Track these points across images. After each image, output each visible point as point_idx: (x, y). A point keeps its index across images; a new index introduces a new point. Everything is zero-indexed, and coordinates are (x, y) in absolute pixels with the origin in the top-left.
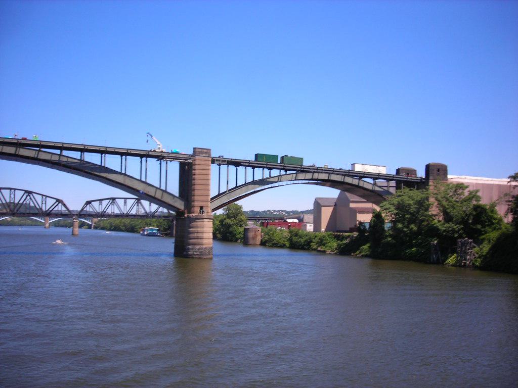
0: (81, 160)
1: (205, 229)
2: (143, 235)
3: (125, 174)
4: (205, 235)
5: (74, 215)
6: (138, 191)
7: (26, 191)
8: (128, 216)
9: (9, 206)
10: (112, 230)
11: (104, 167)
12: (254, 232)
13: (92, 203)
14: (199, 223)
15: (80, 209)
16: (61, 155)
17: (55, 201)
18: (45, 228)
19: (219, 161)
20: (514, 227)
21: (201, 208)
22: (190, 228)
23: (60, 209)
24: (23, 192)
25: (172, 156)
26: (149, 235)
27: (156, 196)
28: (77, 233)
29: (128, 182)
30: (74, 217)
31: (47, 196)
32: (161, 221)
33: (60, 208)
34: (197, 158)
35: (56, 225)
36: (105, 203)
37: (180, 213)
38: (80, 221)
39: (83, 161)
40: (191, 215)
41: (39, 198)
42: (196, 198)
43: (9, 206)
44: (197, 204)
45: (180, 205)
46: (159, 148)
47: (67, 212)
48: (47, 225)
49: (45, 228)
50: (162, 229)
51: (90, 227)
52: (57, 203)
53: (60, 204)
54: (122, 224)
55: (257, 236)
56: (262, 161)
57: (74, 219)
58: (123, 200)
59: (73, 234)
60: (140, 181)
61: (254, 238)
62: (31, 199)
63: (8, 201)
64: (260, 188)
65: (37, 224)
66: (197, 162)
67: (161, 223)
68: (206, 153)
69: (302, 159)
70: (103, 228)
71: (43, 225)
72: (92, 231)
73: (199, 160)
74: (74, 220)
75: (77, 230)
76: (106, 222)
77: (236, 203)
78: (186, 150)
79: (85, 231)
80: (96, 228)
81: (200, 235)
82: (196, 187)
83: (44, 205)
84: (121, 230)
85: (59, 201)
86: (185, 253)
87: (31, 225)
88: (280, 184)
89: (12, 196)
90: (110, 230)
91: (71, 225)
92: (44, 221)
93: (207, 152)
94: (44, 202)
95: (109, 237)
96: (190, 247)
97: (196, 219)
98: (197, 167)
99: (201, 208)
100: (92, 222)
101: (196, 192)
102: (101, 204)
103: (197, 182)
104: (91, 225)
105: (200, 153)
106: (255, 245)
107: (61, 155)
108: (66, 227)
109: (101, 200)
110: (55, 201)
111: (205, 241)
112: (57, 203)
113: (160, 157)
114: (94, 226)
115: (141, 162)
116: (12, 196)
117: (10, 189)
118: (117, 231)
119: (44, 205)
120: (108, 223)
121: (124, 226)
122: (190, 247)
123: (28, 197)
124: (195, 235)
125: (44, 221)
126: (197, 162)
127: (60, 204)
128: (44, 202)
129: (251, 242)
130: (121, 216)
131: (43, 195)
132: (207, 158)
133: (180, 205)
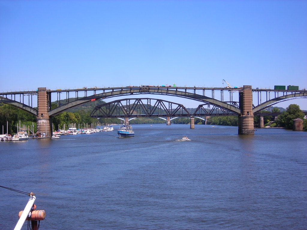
0: (194, 94)
1: (249, 122)
3: (214, 99)
4: (250, 124)
5: (191, 115)
6: (220, 106)
10: (222, 125)
11: (205, 96)
12: (298, 123)
14: (247, 119)
16: (185, 92)
17: (178, 105)
18: (167, 125)
19: (258, 90)
20: (50, 129)
21: (248, 112)
22: (243, 121)
25: (236, 89)
27: (228, 108)
28: (193, 127)
29: (215, 102)
30: (191, 116)
31: (172, 103)
34: (245, 90)
35: (174, 122)
37: (240, 115)
38: (196, 119)
39: (195, 94)
40: (243, 116)
42: (245, 108)
44: (246, 111)
45: (239, 111)
46: (228, 86)
47: (187, 113)
48: (169, 122)
49: (167, 125)
51: (203, 123)
52: (179, 107)
54: (229, 120)
55: (300, 125)
56: (278, 88)
57: (191, 117)
59: (191, 128)
60: (221, 102)
61: (299, 126)
62: (161, 104)
64: (275, 103)
66: (245, 92)
68: (249, 88)
69: (298, 87)
70: (214, 124)
71: (166, 122)
72: (206, 126)
73: (246, 91)
74: (192, 118)
75: (193, 125)
78: (240, 85)
79: (199, 126)
80: (209, 123)
81: (247, 124)
82: (245, 103)
84: (228, 125)
86: (241, 133)
87: (154, 123)
88: (286, 99)
90: (220, 124)
91: (189, 122)
92: (166, 120)
93: (250, 87)
95: (213, 128)
96: (243, 130)
97: (245, 117)
98: (245, 94)
99: (248, 112)
100: (205, 119)
101: (245, 106)
103: (245, 101)
105: (246, 88)
106: (299, 130)
107: (185, 92)
108: (184, 123)
110: (178, 105)
111: (249, 127)
112: (179, 107)
113: (230, 90)
114: (207, 122)
115: (221, 92)
120: (218, 119)
121: (230, 121)
122: (243, 130)
123: (160, 104)
124: (245, 124)
125: (166, 120)
126: (245, 92)
129: (297, 128)
131: (169, 102)
132: (250, 90)
133: (239, 111)
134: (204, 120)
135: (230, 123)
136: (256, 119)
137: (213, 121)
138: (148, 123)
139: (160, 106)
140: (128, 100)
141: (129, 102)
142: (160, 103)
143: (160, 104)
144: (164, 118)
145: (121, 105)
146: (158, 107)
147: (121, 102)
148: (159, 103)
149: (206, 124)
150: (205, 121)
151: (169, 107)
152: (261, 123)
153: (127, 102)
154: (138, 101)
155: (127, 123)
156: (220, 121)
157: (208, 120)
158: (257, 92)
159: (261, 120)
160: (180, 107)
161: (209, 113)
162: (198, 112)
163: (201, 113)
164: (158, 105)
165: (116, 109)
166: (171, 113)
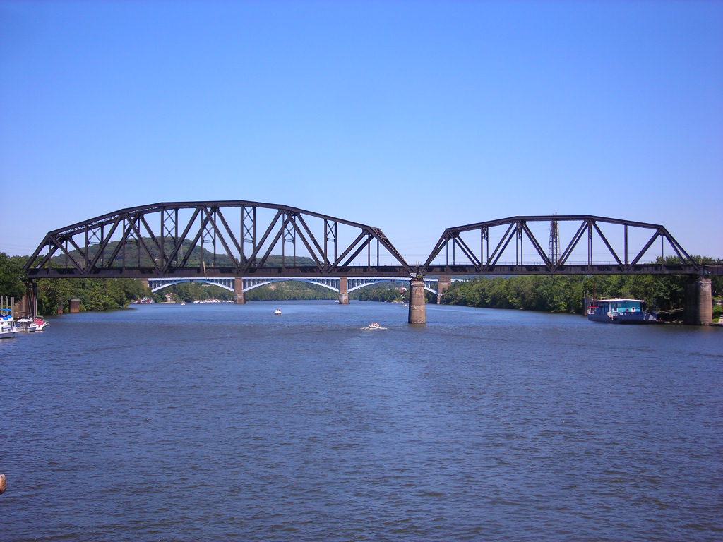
2: (601, 318)
7: (282, 209)
8: (492, 269)
9: (160, 248)
13: (461, 235)
15: (30, 254)
17: (360, 231)
18: (341, 303)
23: (289, 253)
24: (276, 211)
26: (618, 320)
28: (422, 318)
30: (414, 275)
31: (337, 221)
32: (649, 279)
33: (376, 255)
35: (364, 296)
36: (496, 233)
41: (316, 226)
43: (160, 248)
47: (396, 263)
48: (345, 297)
49: (341, 303)
50: (652, 302)
52: (366, 237)
53: (374, 241)
54: (513, 292)
57: (414, 279)
58: (548, 224)
59: (410, 322)
62: (296, 228)
63: (157, 234)
65: (325, 296)
67: (647, 286)
70: (463, 302)
74: (414, 283)
76: (496, 284)
77: (109, 242)
80: (446, 301)
83: (331, 245)
84: (511, 307)
85: (371, 232)
87: (315, 299)
89: (248, 223)
90: (482, 305)
94: (331, 236)
100: (437, 290)
102: (485, 235)
104: (435, 296)
108: (383, 300)
109: (484, 227)
110: (360, 231)
112: (366, 237)
114: (442, 297)
116: (248, 223)
117: (242, 204)
118: (500, 307)
119: (331, 245)
120: (477, 290)
123: (290, 226)
127: (374, 241)
128: (331, 236)
130: (476, 269)
131: (326, 218)
134: (434, 292)
135: (516, 301)
136: (665, 288)
137: (458, 294)
138: (274, 297)
139: (292, 232)
140: (249, 209)
141: (251, 214)
142: (294, 222)
143: (290, 226)
144: (329, 285)
145: (144, 233)
146: (199, 243)
147: (146, 216)
148: (285, 224)
149: (438, 303)
150: (435, 296)
151: (326, 235)
152: (702, 305)
153: (245, 214)
154: (209, 214)
155: (239, 296)
156: (484, 297)
157: (444, 292)
158: (239, 209)
159: (702, 293)
160: (371, 238)
161: (484, 264)
162: (439, 260)
163: (374, 263)
164: (200, 235)
165: (281, 239)
166: (332, 261)
